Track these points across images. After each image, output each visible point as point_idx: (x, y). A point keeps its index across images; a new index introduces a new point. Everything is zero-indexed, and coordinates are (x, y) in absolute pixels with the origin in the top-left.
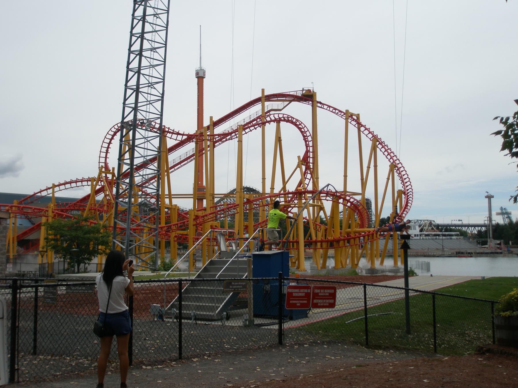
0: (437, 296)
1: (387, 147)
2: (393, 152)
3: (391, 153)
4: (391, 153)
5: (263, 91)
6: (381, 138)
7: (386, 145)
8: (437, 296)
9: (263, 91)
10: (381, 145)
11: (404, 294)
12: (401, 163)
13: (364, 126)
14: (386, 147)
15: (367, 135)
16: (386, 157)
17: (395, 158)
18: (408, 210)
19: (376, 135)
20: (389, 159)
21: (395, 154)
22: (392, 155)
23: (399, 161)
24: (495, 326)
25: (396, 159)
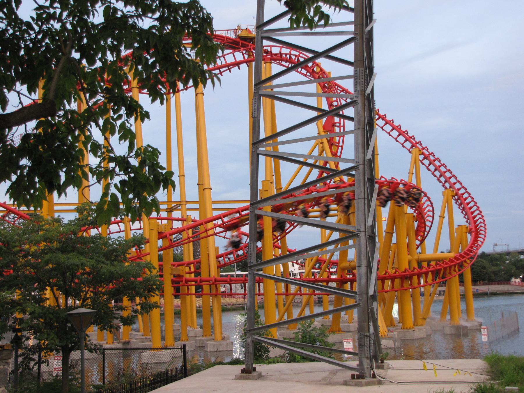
0: (423, 368)
1: (427, 150)
2: (433, 153)
3: (434, 161)
4: (434, 161)
5: (239, 69)
6: (413, 136)
7: (424, 147)
8: (423, 368)
9: (239, 69)
10: (383, 120)
11: (341, 321)
12: (459, 182)
13: (383, 117)
14: (424, 151)
15: (389, 133)
16: (433, 174)
17: (443, 169)
18: (222, 59)
19: (397, 127)
20: (433, 170)
21: (448, 168)
22: (437, 163)
23: (451, 173)
24: (322, 296)
25: (450, 175)
